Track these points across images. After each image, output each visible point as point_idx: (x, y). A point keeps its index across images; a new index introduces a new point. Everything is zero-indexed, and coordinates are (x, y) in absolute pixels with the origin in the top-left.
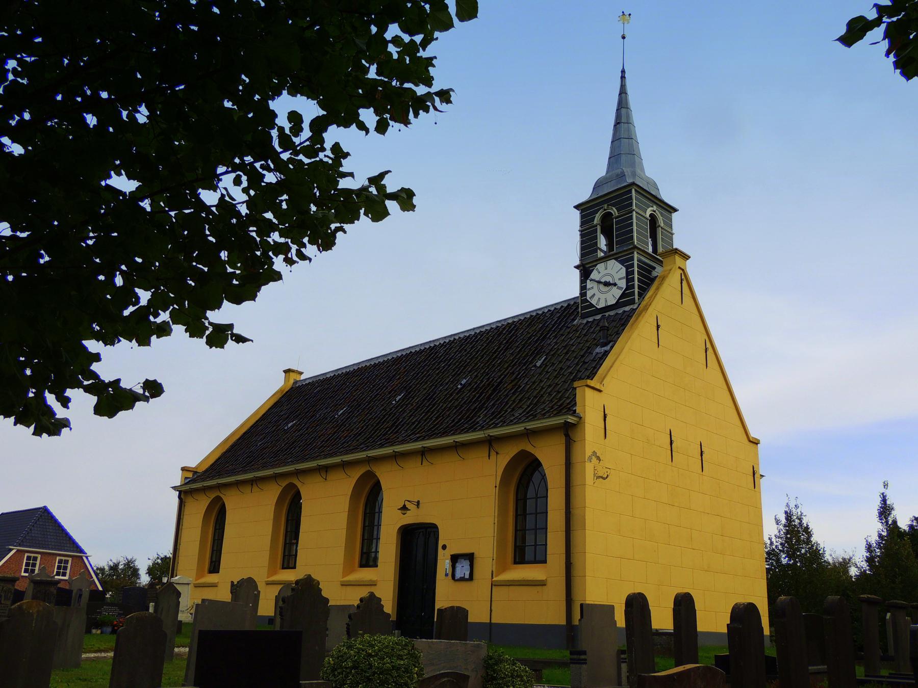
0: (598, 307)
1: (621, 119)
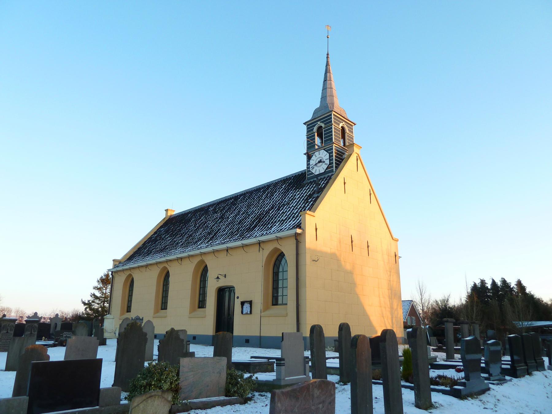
0: (316, 174)
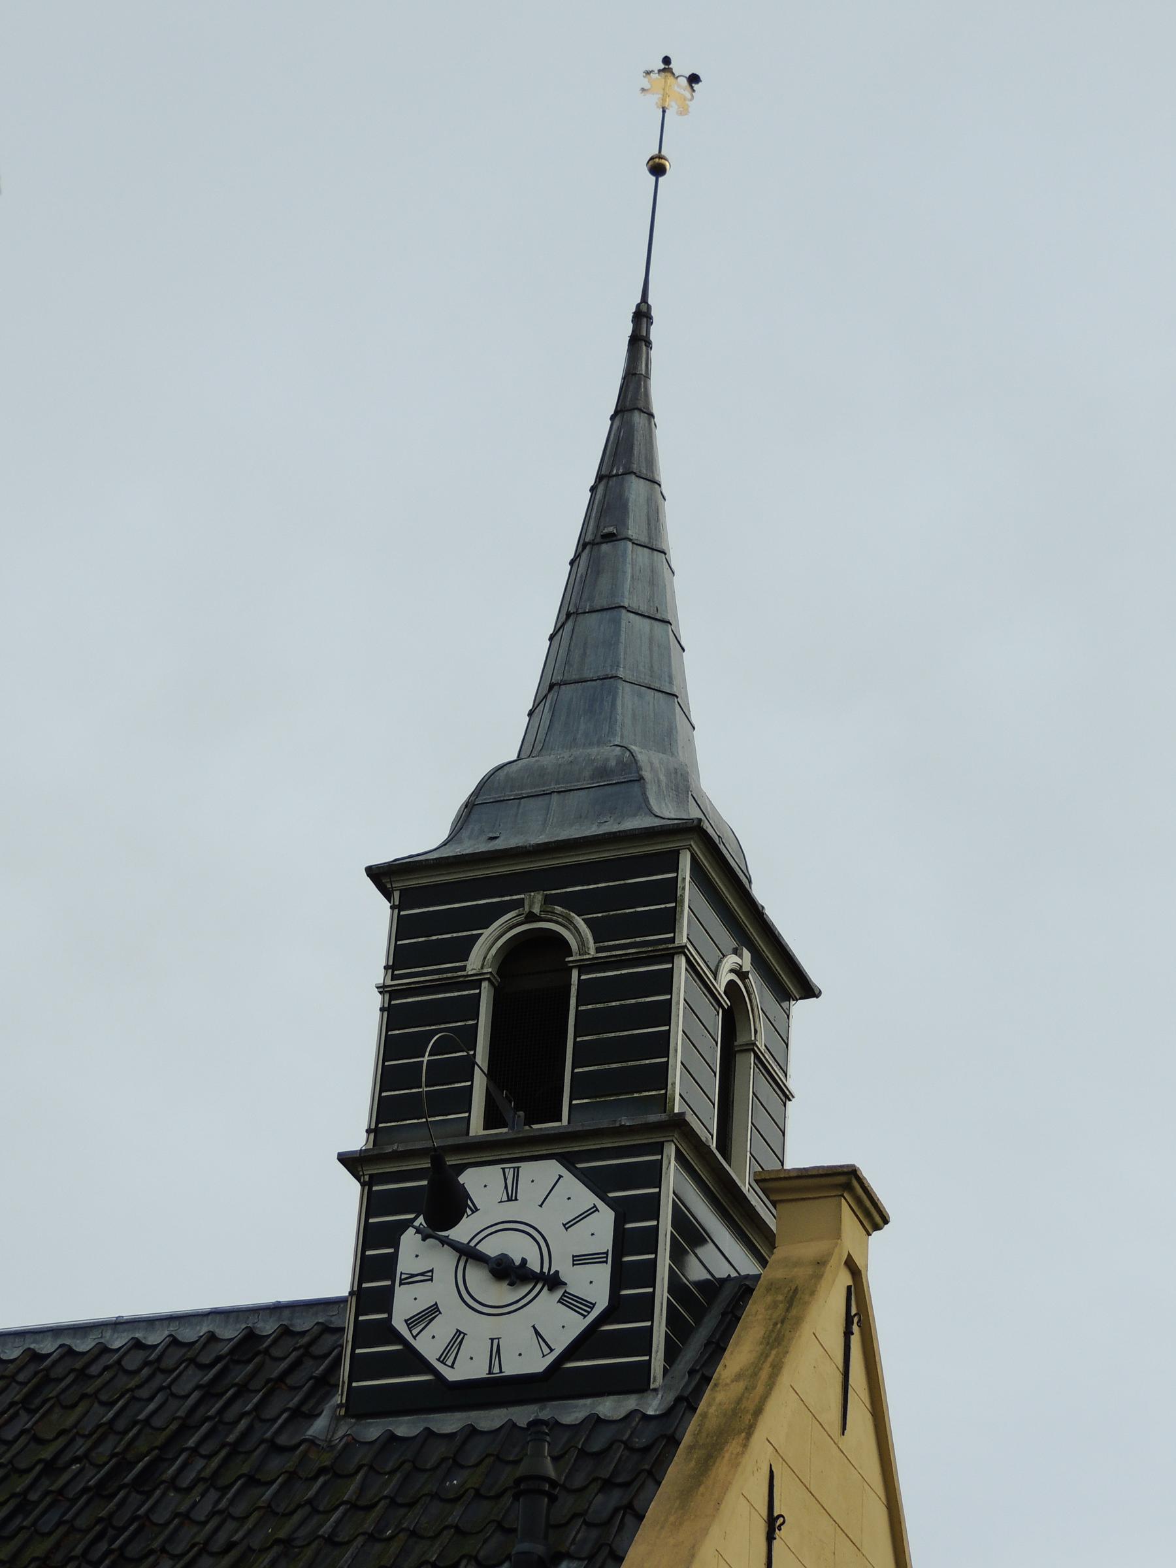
0: (451, 1375)
1: (623, 521)
